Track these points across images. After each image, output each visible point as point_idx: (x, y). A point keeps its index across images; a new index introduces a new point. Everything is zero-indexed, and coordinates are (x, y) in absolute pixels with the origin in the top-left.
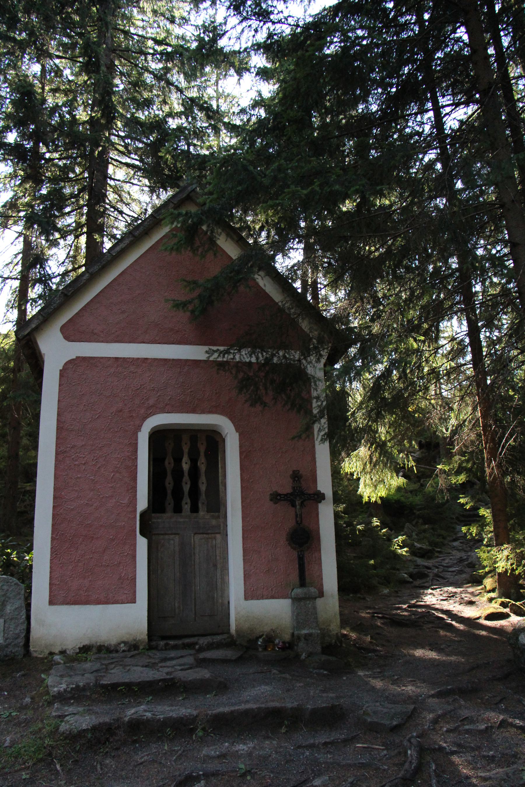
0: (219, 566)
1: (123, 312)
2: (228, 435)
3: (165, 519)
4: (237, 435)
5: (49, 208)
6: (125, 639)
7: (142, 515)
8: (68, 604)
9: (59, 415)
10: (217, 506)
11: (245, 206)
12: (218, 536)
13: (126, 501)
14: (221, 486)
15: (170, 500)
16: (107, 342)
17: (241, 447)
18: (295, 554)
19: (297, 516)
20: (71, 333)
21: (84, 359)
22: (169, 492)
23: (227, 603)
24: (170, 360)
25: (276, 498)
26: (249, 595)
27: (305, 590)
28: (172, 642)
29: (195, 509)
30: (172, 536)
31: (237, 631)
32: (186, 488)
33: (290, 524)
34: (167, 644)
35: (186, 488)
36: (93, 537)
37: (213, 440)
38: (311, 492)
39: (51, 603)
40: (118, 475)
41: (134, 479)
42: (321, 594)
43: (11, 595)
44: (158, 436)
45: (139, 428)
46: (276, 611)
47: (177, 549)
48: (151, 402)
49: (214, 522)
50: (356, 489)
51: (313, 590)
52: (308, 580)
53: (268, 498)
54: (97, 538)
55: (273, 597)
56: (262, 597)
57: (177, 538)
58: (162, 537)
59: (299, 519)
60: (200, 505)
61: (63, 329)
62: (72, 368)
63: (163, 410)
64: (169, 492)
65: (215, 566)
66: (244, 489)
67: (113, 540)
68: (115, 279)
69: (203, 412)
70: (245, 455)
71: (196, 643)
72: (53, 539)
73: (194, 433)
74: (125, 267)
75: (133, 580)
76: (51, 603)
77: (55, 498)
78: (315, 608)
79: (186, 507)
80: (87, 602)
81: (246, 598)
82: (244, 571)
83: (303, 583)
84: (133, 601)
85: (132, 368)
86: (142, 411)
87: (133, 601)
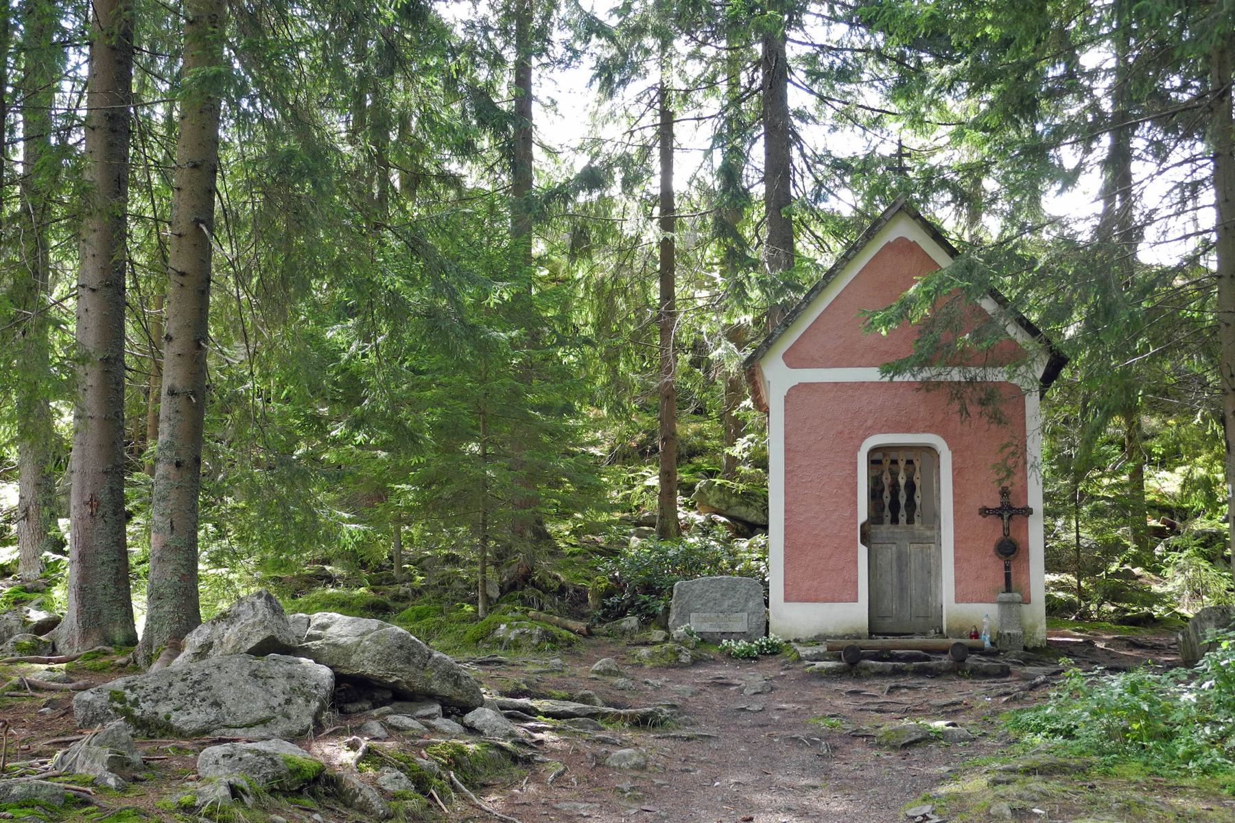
3: (885, 529)
4: (950, 453)
7: (862, 526)
10: (934, 519)
13: (847, 514)
15: (887, 513)
17: (953, 464)
18: (1002, 564)
20: (794, 359)
21: (806, 385)
22: (887, 509)
25: (985, 512)
26: (959, 599)
27: (1009, 595)
29: (910, 521)
32: (903, 501)
33: (998, 535)
35: (903, 501)
38: (1021, 506)
39: (786, 600)
41: (855, 494)
42: (1027, 600)
45: (858, 447)
46: (984, 615)
47: (894, 557)
48: (869, 423)
49: (928, 533)
52: (1013, 586)
55: (981, 602)
56: (971, 601)
57: (894, 548)
61: (785, 356)
62: (796, 394)
63: (880, 432)
64: (887, 509)
66: (955, 484)
69: (917, 432)
70: (958, 472)
72: (785, 547)
76: (786, 600)
79: (903, 518)
80: (816, 600)
83: (1008, 589)
84: (856, 600)
85: (850, 392)
87: (856, 600)
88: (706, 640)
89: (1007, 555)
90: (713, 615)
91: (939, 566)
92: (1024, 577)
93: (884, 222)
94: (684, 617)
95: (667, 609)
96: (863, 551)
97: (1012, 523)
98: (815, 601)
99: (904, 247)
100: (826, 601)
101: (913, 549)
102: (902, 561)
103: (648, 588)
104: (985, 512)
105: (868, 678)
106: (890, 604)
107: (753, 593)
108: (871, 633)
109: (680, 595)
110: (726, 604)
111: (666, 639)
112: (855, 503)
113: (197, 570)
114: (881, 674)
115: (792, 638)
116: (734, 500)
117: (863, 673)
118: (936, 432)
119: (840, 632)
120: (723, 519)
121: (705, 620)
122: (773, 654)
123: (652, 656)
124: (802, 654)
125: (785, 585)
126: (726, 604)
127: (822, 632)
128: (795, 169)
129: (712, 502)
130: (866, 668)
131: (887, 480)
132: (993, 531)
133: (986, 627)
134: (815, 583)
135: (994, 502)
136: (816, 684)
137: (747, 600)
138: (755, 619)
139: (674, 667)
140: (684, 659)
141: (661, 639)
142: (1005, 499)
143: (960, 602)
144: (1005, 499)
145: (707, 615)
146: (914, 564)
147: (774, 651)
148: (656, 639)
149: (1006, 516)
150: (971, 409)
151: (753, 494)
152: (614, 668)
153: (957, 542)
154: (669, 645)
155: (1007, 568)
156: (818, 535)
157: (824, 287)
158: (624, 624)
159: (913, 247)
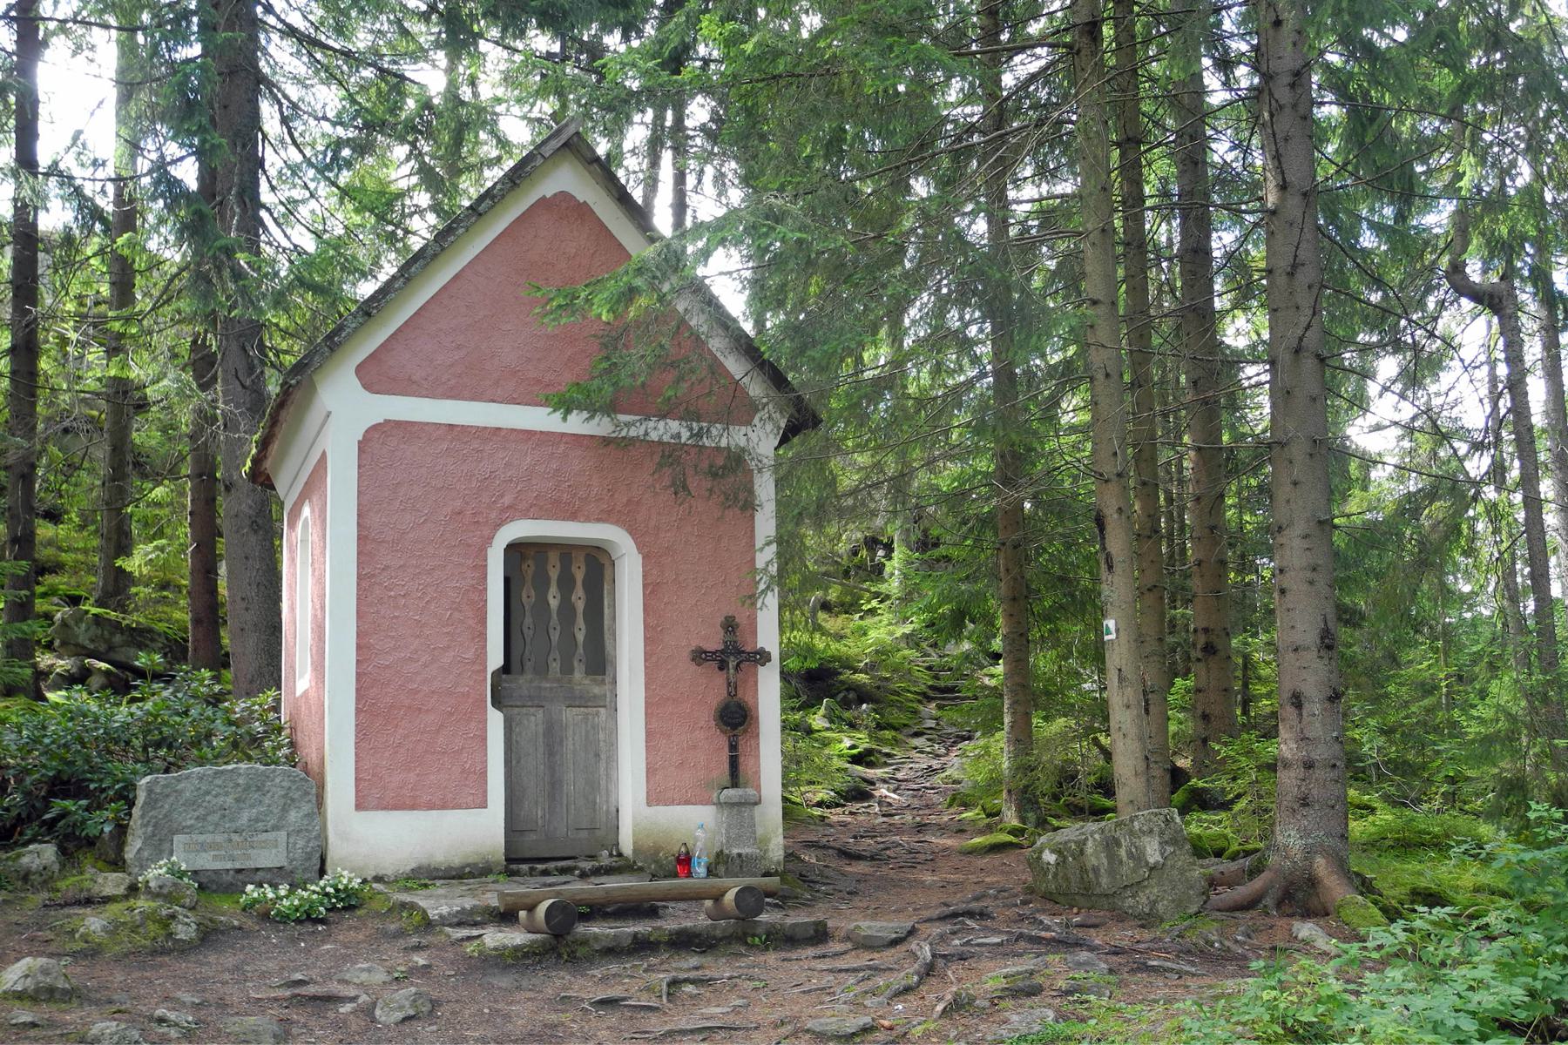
1: (459, 347)
2: (626, 558)
3: (522, 683)
5: (454, 162)
6: (470, 861)
9: (360, 515)
10: (600, 662)
12: (602, 710)
14: (607, 636)
16: (434, 397)
19: (729, 684)
20: (375, 377)
21: (398, 424)
24: (535, 432)
25: (700, 656)
26: (655, 797)
28: (540, 867)
29: (568, 669)
31: (635, 851)
34: (532, 869)
37: (597, 560)
39: (359, 806)
40: (457, 615)
41: (483, 621)
44: (516, 551)
45: (489, 540)
46: (695, 823)
47: (541, 729)
48: (507, 500)
49: (596, 690)
51: (751, 791)
53: (686, 654)
55: (687, 803)
56: (672, 802)
58: (516, 710)
59: (732, 687)
60: (576, 664)
61: (359, 370)
63: (525, 515)
65: (597, 755)
68: (444, 288)
69: (588, 520)
70: (652, 590)
71: (575, 868)
72: (358, 711)
73: (567, 550)
74: (459, 268)
76: (359, 806)
77: (359, 647)
78: (752, 818)
79: (555, 666)
81: (649, 804)
83: (735, 779)
84: (483, 805)
86: (493, 515)
87: (483, 805)
88: (209, 885)
89: (734, 727)
90: (219, 838)
91: (613, 744)
92: (752, 762)
93: (539, 161)
94: (159, 844)
95: (121, 830)
96: (495, 721)
97: (741, 675)
98: (413, 807)
99: (566, 208)
100: (431, 806)
101: (570, 715)
102: (552, 737)
103: (63, 786)
104: (700, 656)
105: (590, 960)
106: (535, 811)
107: (296, 796)
108: (509, 860)
109: (151, 802)
110: (244, 818)
111: (133, 890)
112: (482, 636)
114: (612, 951)
115: (370, 875)
116: (118, 638)
117: (581, 952)
118: (617, 523)
119: (457, 861)
120: (104, 666)
121: (204, 847)
122: (349, 908)
123: (114, 929)
124: (433, 914)
126: (244, 818)
127: (425, 862)
128: (265, 137)
129: (83, 639)
130: (584, 942)
131: (579, 599)
132: (713, 689)
133: (699, 844)
134: (412, 777)
135: (714, 643)
136: (504, 981)
137: (285, 810)
138: (301, 843)
139: (164, 952)
140: (185, 930)
141: (121, 890)
142: (729, 638)
143: (643, 798)
144: (729, 638)
145: (208, 838)
146: (572, 743)
147: (348, 903)
148: (108, 890)
149: (732, 663)
150: (692, 483)
151: (150, 630)
152: (61, 984)
153: (652, 706)
154: (143, 904)
155: (733, 747)
156: (416, 692)
157: (435, 256)
158: (25, 860)
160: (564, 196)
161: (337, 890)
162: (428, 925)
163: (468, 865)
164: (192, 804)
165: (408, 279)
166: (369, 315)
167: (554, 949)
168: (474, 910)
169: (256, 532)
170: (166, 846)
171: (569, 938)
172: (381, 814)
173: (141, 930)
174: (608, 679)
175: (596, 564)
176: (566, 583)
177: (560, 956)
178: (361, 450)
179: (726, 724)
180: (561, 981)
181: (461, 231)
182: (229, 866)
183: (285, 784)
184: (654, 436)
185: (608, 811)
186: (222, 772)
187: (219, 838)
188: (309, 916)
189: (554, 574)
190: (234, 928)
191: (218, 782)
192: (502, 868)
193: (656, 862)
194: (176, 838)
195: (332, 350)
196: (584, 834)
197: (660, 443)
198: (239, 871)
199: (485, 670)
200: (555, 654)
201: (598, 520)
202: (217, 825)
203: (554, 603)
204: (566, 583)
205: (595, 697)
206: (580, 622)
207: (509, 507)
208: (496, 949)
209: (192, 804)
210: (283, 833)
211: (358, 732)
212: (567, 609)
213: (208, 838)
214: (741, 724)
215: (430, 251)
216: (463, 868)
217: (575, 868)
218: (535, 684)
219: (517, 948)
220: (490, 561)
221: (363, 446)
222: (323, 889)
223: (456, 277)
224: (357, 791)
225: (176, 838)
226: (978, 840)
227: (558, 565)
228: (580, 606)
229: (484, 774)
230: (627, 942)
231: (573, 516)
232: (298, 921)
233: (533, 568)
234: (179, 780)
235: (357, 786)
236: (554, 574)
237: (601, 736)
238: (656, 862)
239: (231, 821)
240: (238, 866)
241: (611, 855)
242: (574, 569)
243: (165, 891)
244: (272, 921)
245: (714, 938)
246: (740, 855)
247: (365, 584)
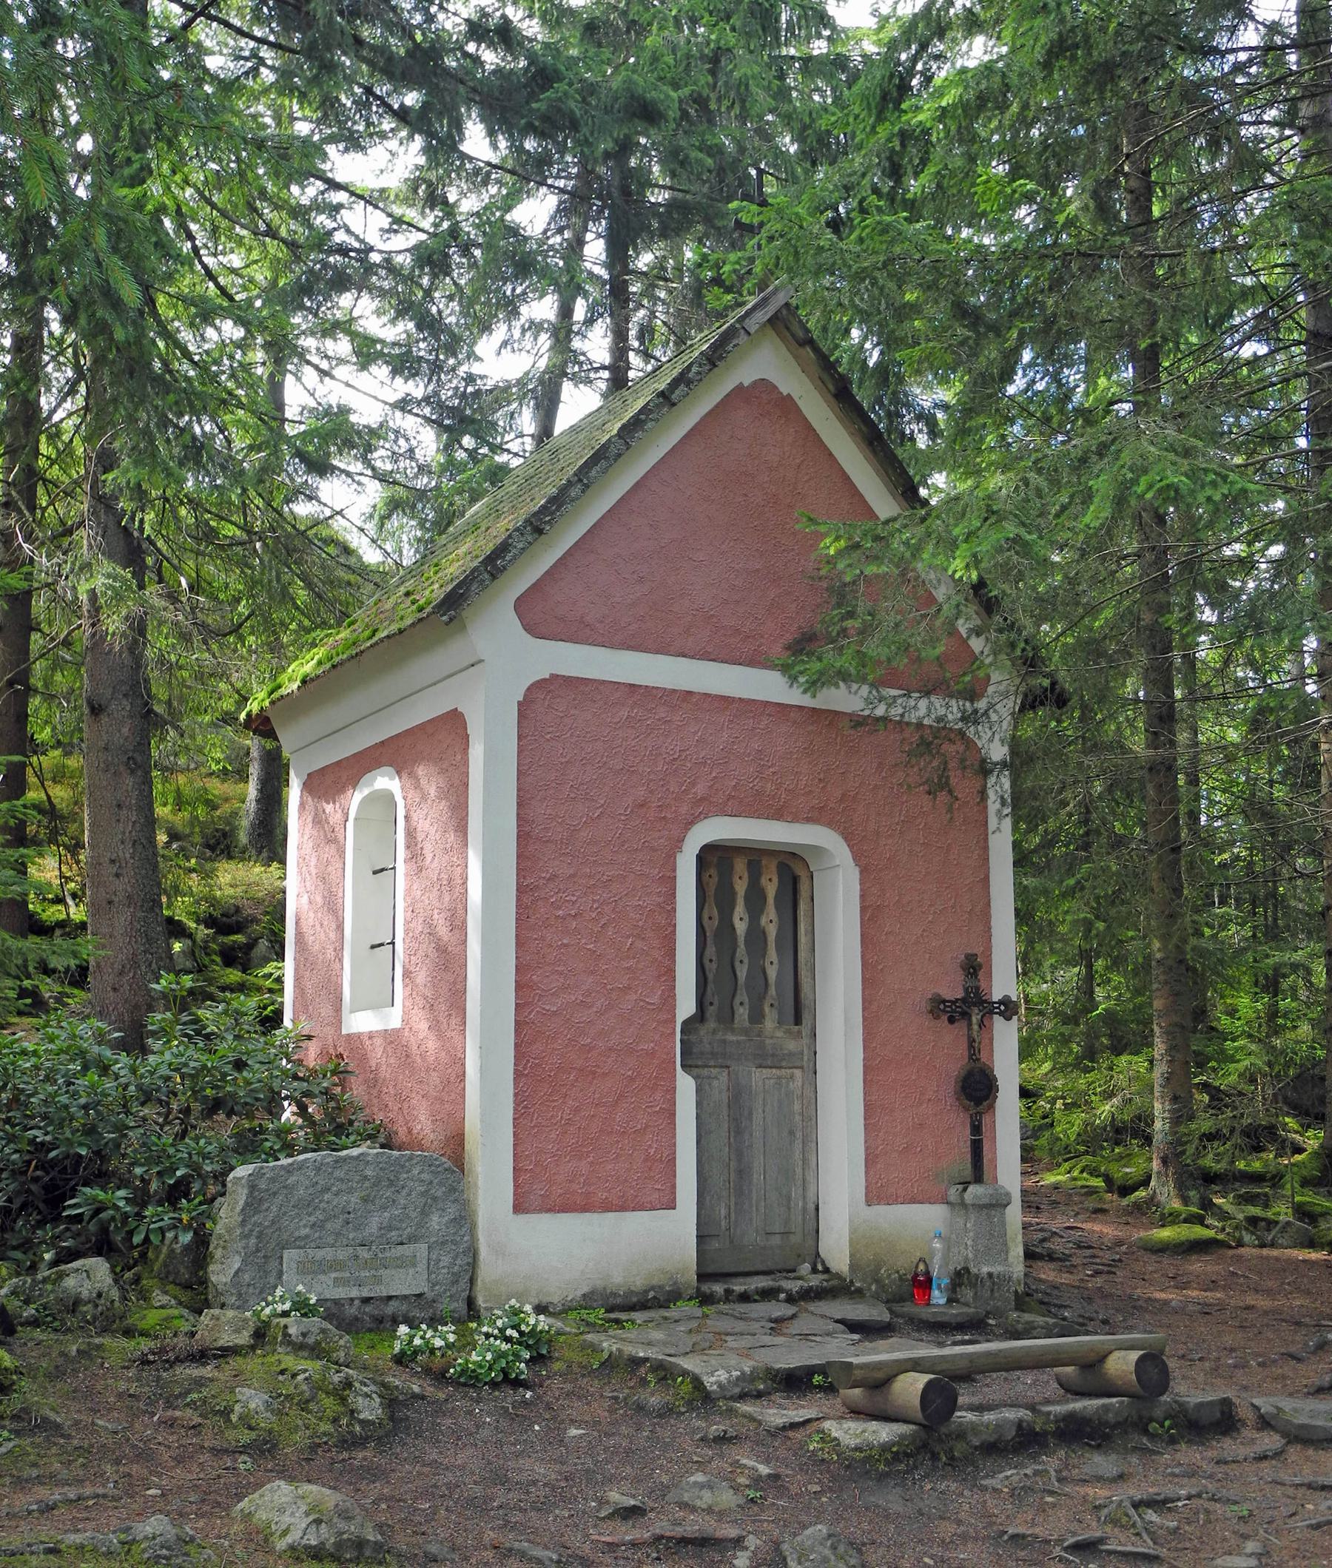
0: (799, 1134)
1: (641, 580)
4: (857, 871)
6: (655, 1282)
8: (549, 1210)
11: (572, 278)
12: (798, 1073)
13: (655, 999)
17: (863, 897)
20: (539, 617)
23: (811, 1207)
26: (875, 1195)
30: (714, 1071)
31: (851, 1266)
34: (728, 1292)
36: (594, 1073)
40: (639, 944)
41: (671, 953)
43: (439, 1194)
44: (712, 857)
45: (678, 843)
46: (922, 1228)
48: (700, 789)
49: (791, 1045)
50: (276, 927)
54: (605, 1074)
57: (724, 1076)
60: (767, 1009)
65: (792, 1133)
67: (632, 1079)
69: (795, 819)
70: (871, 914)
72: (518, 1075)
73: (755, 855)
75: (671, 1163)
76: (519, 1208)
77: (519, 987)
79: (742, 1013)
81: (869, 1203)
82: (867, 1149)
85: (662, 712)
86: (684, 809)
89: (978, 1102)
90: (342, 1254)
93: (742, 339)
96: (686, 1085)
98: (585, 1209)
99: (761, 397)
100: (607, 1207)
101: (758, 1078)
108: (702, 1277)
112: (669, 973)
113: (581, 257)
118: (829, 824)
119: (639, 1283)
125: (517, 1171)
127: (599, 1284)
131: (770, 920)
132: (947, 1048)
135: (952, 990)
137: (425, 1213)
138: (446, 1260)
141: (244, 1338)
145: (327, 1253)
153: (874, 1070)
155: (976, 1129)
158: (70, 1282)
159: (787, 406)
160: (763, 385)
161: (521, 1333)
162: (702, 1398)
163: (653, 1288)
164: (308, 1205)
165: (587, 486)
166: (539, 531)
167: (925, 1446)
168: (753, 1377)
169: (133, 772)
170: (273, 1264)
171: (944, 1430)
172: (548, 1215)
173: (312, 1406)
174: (805, 1029)
175: (792, 872)
176: (756, 900)
177: (935, 1457)
178: (522, 715)
179: (970, 1097)
180: (936, 1490)
181: (650, 425)
182: (354, 1293)
183: (425, 1176)
184: (913, 717)
185: (804, 1210)
186: (345, 1159)
187: (342, 1254)
188: (506, 1378)
189: (741, 887)
190: (415, 1396)
191: (337, 1173)
192: (692, 1292)
193: (877, 1281)
194: (286, 1254)
195: (494, 577)
196: (776, 1240)
197: (920, 725)
198: (366, 1301)
199: (673, 1020)
200: (742, 996)
201: (809, 820)
202: (338, 1234)
203: (741, 927)
204: (756, 900)
205: (791, 1054)
206: (772, 954)
207: (703, 799)
208: (857, 1449)
209: (308, 1205)
210: (422, 1248)
211: (517, 1104)
212: (756, 936)
213: (327, 1253)
214: (986, 1098)
215: (613, 450)
216: (646, 1292)
217: (779, 1290)
218: (719, 1036)
219: (885, 1448)
220: (680, 873)
221: (524, 708)
222: (502, 1330)
223: (637, 486)
224: (517, 1186)
225: (286, 1254)
226: (1166, 1234)
227: (746, 875)
228: (772, 931)
229: (672, 1161)
230: (1010, 1434)
231: (778, 814)
232: (494, 1385)
233: (716, 879)
234: (289, 1170)
235: (515, 1179)
236: (741, 887)
237: (797, 1107)
238: (877, 1281)
239: (356, 1229)
240: (365, 1294)
241: (814, 1271)
242: (764, 881)
243: (311, 1340)
244: (454, 1382)
245: (1106, 1424)
246: (990, 1275)
247: (527, 900)
